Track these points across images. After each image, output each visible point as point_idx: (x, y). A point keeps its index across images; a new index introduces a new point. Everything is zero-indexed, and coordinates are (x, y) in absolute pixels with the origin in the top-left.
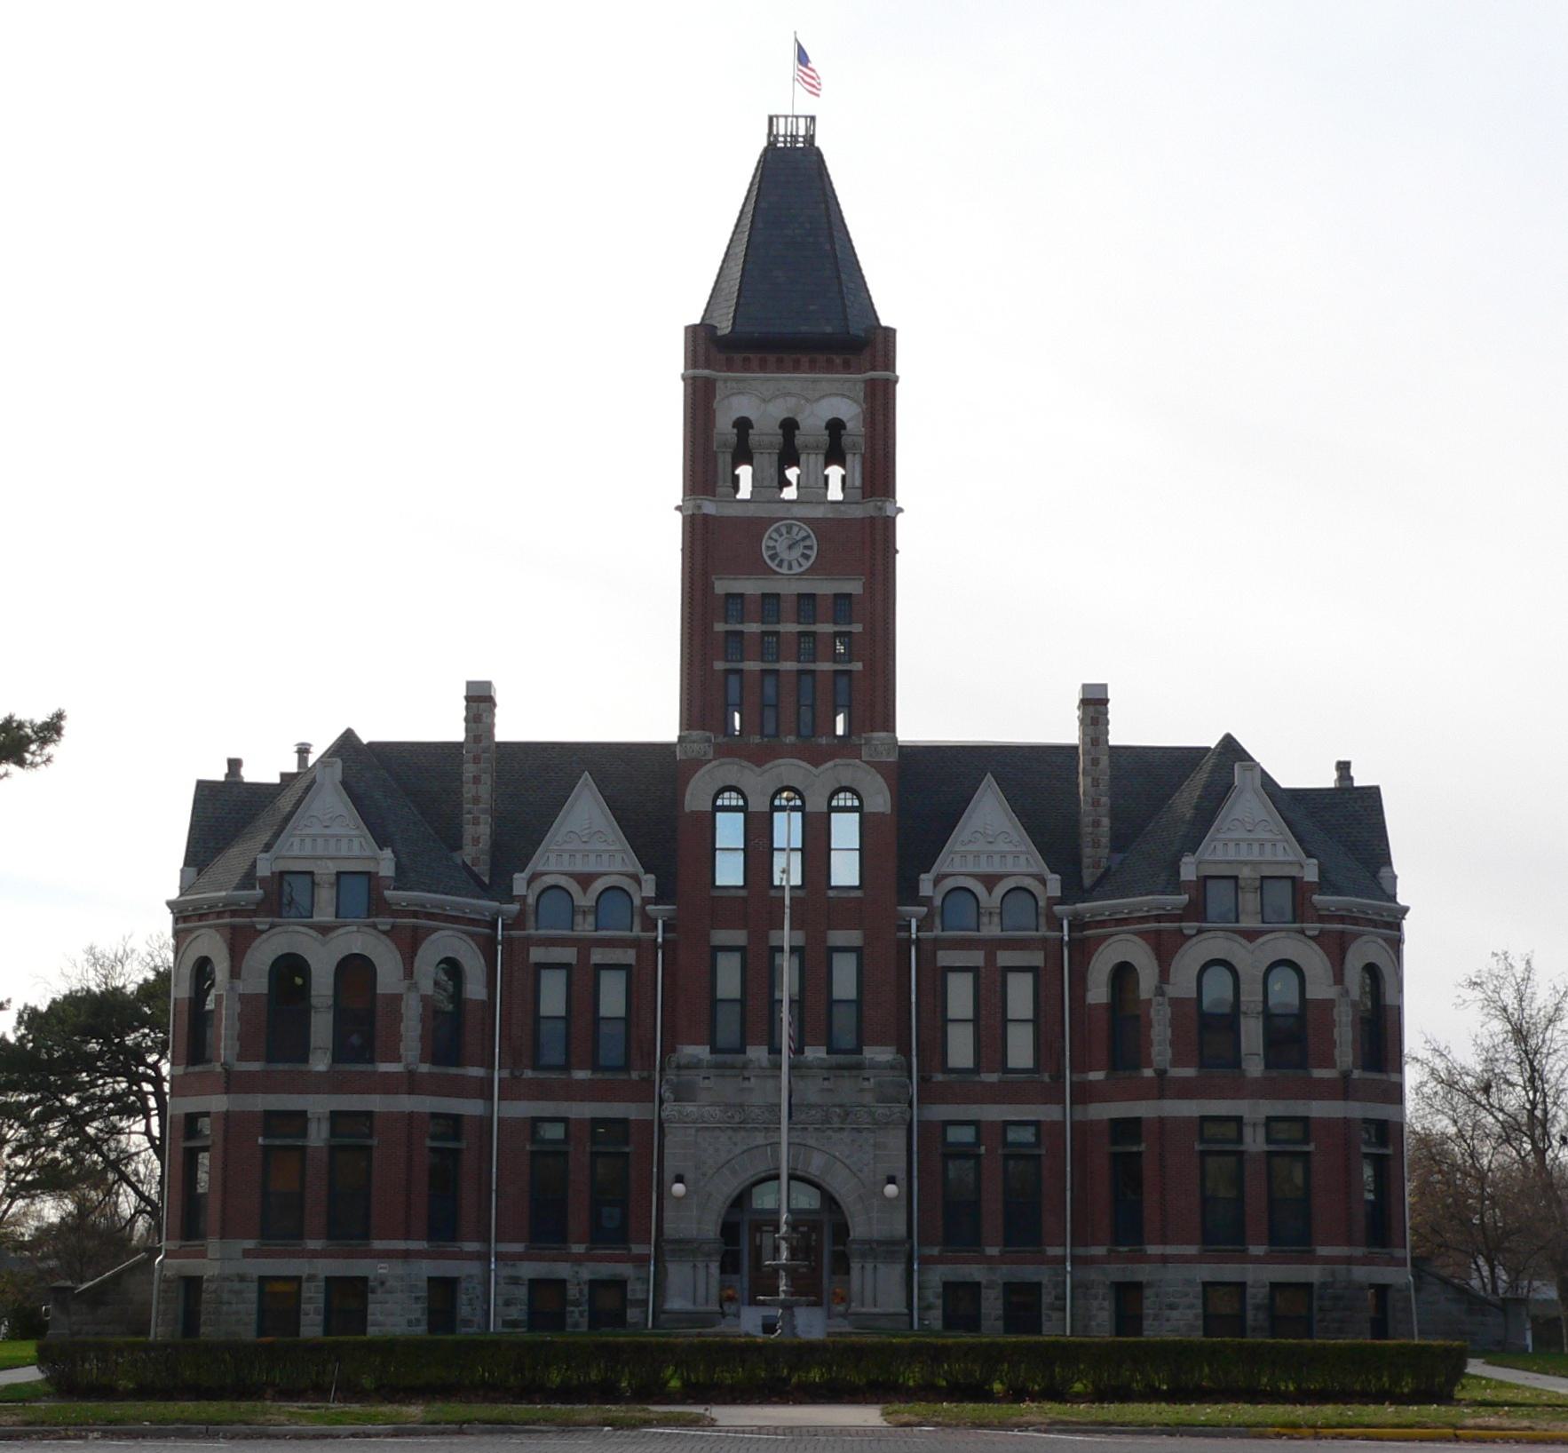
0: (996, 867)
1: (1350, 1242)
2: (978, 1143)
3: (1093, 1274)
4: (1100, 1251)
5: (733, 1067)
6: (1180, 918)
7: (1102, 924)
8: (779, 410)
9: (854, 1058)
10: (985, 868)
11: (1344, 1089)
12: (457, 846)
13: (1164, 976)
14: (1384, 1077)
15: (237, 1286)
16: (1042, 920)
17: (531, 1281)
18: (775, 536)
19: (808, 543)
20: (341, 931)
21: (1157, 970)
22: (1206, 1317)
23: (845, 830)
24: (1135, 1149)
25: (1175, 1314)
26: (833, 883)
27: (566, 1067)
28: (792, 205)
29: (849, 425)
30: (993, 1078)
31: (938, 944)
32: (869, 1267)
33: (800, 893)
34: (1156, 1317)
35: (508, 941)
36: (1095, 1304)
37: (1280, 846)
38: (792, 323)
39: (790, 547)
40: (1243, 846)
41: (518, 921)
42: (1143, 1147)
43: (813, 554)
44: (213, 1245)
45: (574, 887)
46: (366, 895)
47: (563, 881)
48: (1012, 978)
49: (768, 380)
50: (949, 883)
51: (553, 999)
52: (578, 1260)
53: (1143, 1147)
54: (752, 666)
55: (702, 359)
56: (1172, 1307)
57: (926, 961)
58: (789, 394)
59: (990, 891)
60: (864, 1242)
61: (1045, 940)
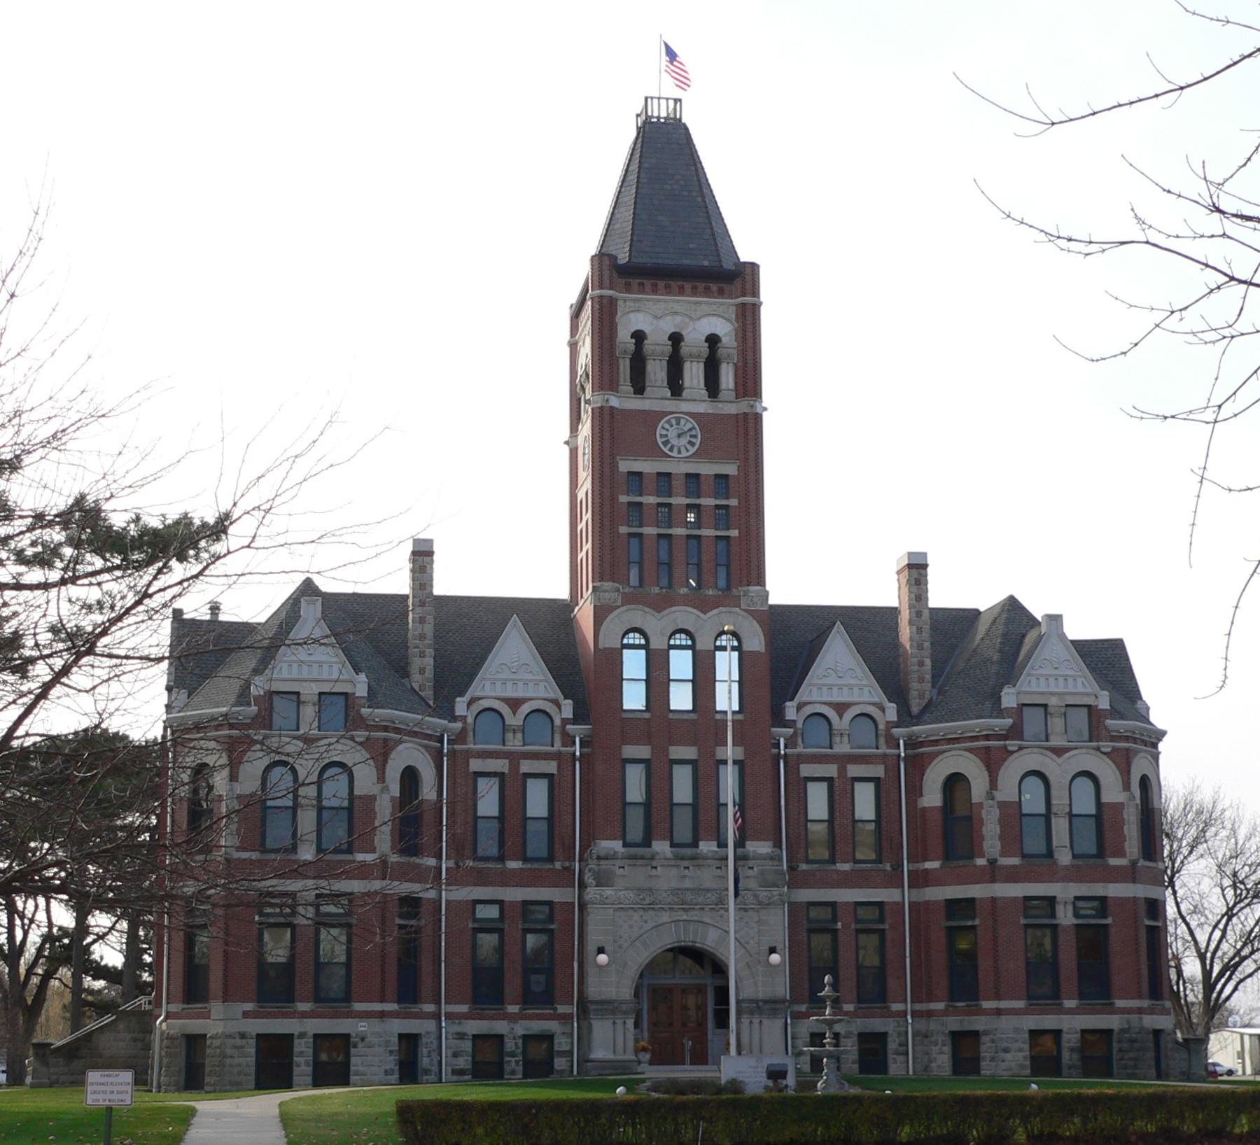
0: (519, 693)
1: (1140, 997)
2: (835, 921)
3: (934, 1025)
4: (940, 1006)
5: (642, 858)
6: (1005, 737)
7: (936, 742)
8: (668, 326)
9: (688, 851)
10: (510, 693)
11: (1131, 874)
12: (406, 675)
13: (993, 784)
14: (418, 861)
15: (238, 1042)
16: (882, 740)
17: (474, 1036)
18: (667, 426)
19: (693, 433)
20: (1071, 753)
21: (987, 778)
22: (1033, 1059)
23: (727, 666)
24: (970, 923)
25: (1008, 1056)
26: (625, 707)
27: (501, 858)
28: (664, 163)
29: (724, 340)
30: (846, 867)
31: (802, 758)
32: (756, 1021)
33: (740, 717)
34: (992, 1059)
35: (452, 754)
36: (935, 1049)
37: (1079, 680)
38: (669, 258)
39: (679, 436)
40: (1052, 680)
41: (460, 737)
42: (977, 922)
43: (698, 442)
44: (216, 1008)
45: (505, 709)
46: (343, 710)
47: (497, 705)
48: (482, 783)
49: (659, 301)
50: (808, 710)
51: (488, 805)
52: (512, 1018)
53: (977, 922)
54: (650, 531)
55: (607, 282)
56: (1006, 1050)
57: (792, 771)
58: (676, 313)
59: (841, 716)
60: (752, 1001)
61: (885, 755)
